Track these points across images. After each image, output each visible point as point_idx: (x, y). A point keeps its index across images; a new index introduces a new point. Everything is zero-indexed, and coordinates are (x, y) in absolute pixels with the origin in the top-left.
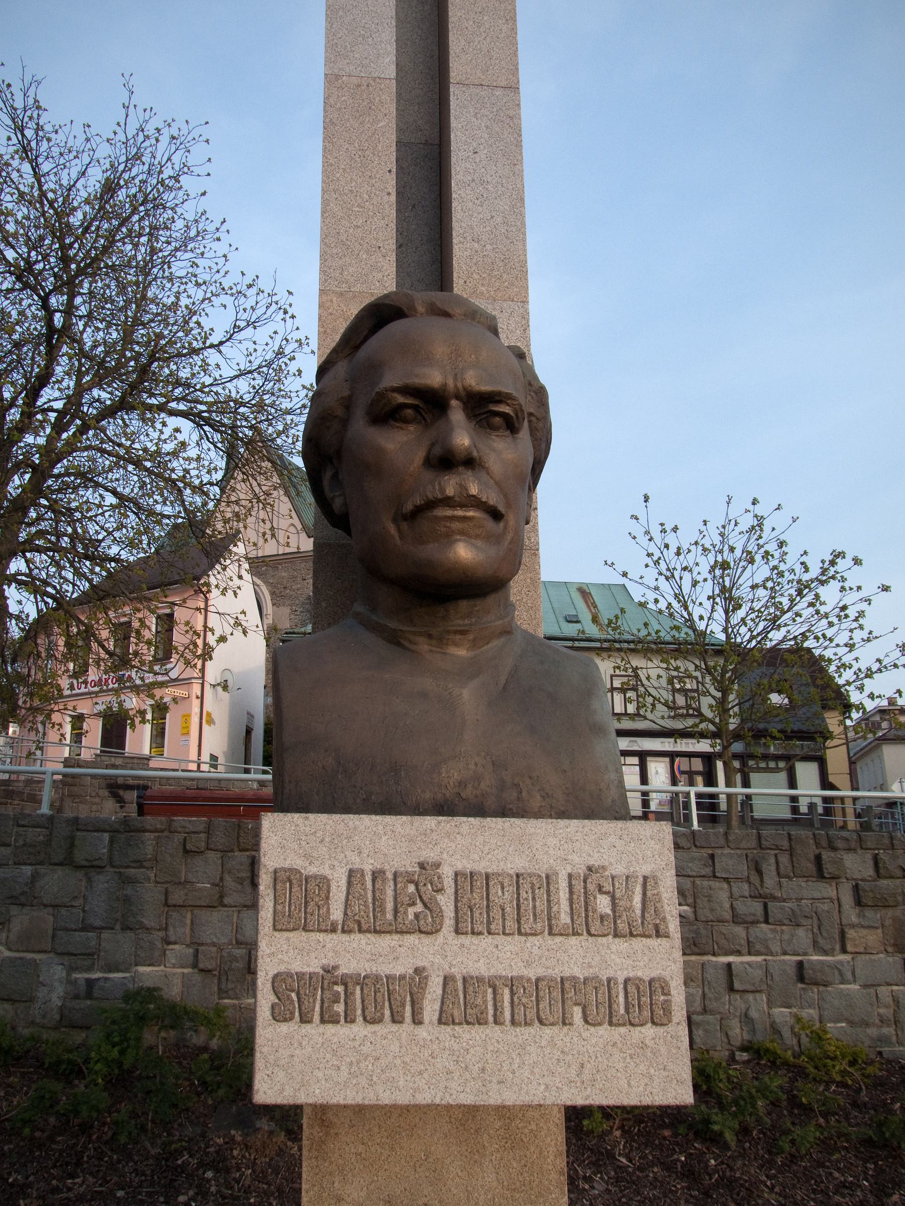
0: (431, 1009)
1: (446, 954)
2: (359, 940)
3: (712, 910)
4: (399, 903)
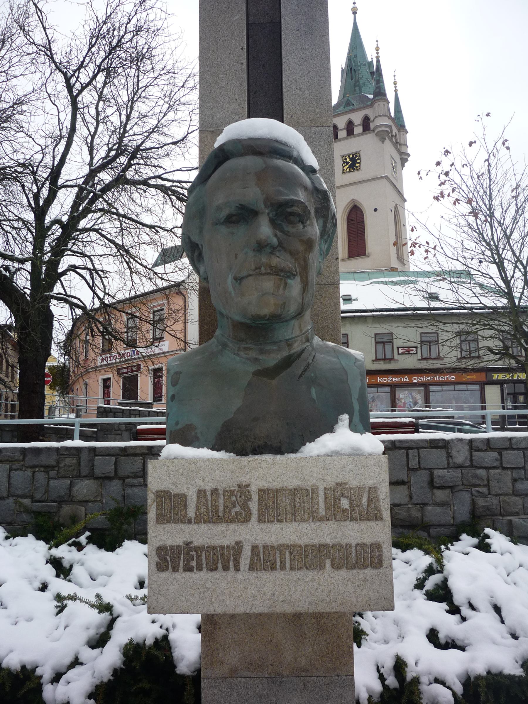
0: (245, 563)
1: (255, 533)
2: (204, 527)
3: (500, 488)
4: (226, 505)
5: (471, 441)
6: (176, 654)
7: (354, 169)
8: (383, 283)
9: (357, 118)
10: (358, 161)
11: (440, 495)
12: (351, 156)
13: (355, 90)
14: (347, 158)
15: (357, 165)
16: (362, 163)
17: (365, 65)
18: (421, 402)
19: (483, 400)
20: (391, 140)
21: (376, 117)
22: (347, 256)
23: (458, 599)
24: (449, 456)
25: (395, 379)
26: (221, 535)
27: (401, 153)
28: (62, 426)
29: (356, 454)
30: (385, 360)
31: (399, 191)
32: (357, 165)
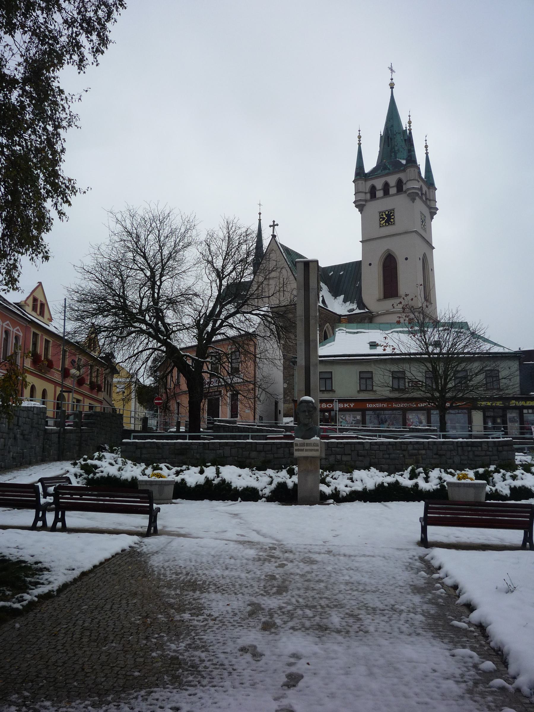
4: (303, 445)
5: (371, 442)
6: (288, 485)
7: (389, 224)
8: (401, 332)
9: (392, 180)
10: (393, 217)
11: (360, 458)
12: (387, 213)
13: (391, 156)
14: (384, 214)
15: (392, 220)
16: (396, 219)
17: (400, 133)
18: (424, 422)
19: (470, 421)
20: (421, 198)
21: (407, 181)
22: (382, 297)
23: (354, 479)
24: (364, 447)
25: (406, 405)
26: (302, 448)
27: (430, 208)
28: (461, 440)
29: (316, 440)
30: (398, 390)
31: (427, 241)
32: (392, 220)
